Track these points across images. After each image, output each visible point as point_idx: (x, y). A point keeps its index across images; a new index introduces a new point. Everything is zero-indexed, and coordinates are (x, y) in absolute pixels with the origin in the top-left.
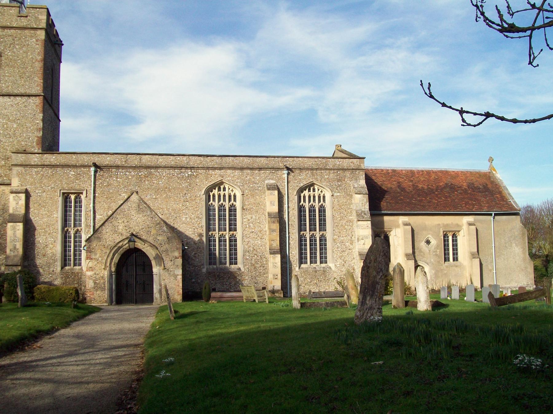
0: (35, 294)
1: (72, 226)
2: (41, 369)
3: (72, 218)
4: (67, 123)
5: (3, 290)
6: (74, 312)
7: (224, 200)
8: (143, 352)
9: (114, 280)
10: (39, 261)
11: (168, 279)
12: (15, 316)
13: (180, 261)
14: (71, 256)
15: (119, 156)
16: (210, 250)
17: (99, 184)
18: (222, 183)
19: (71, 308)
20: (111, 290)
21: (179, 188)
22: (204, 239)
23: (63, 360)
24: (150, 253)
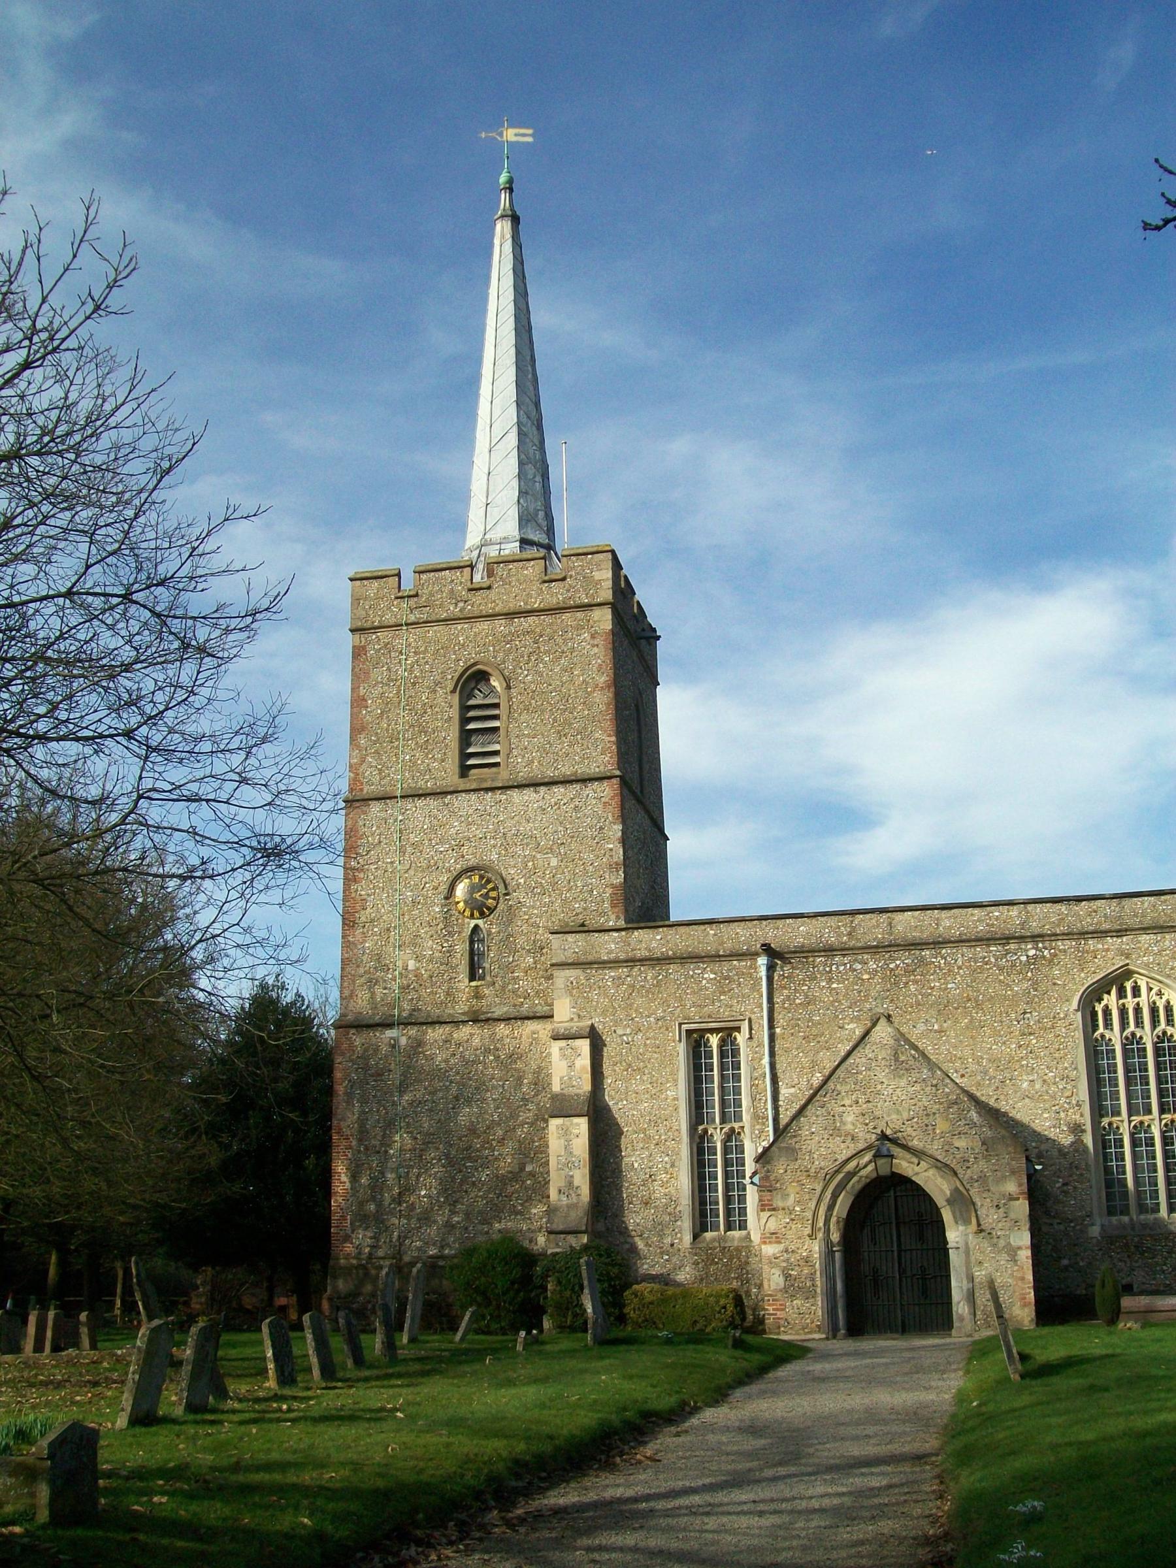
0: (626, 1311)
1: (717, 1120)
2: (663, 1522)
3: (716, 1098)
4: (684, 843)
5: (546, 1298)
6: (736, 1359)
7: (1139, 1023)
8: (940, 1478)
9: (837, 1265)
10: (635, 1219)
11: (991, 1258)
12: (586, 1371)
13: (1022, 1207)
14: (717, 1203)
15: (832, 921)
16: (1107, 1170)
17: (784, 1002)
18: (1128, 974)
19: (726, 1347)
20: (831, 1294)
21: (1005, 998)
22: (1088, 1140)
23: (720, 1497)
24: (937, 1186)
